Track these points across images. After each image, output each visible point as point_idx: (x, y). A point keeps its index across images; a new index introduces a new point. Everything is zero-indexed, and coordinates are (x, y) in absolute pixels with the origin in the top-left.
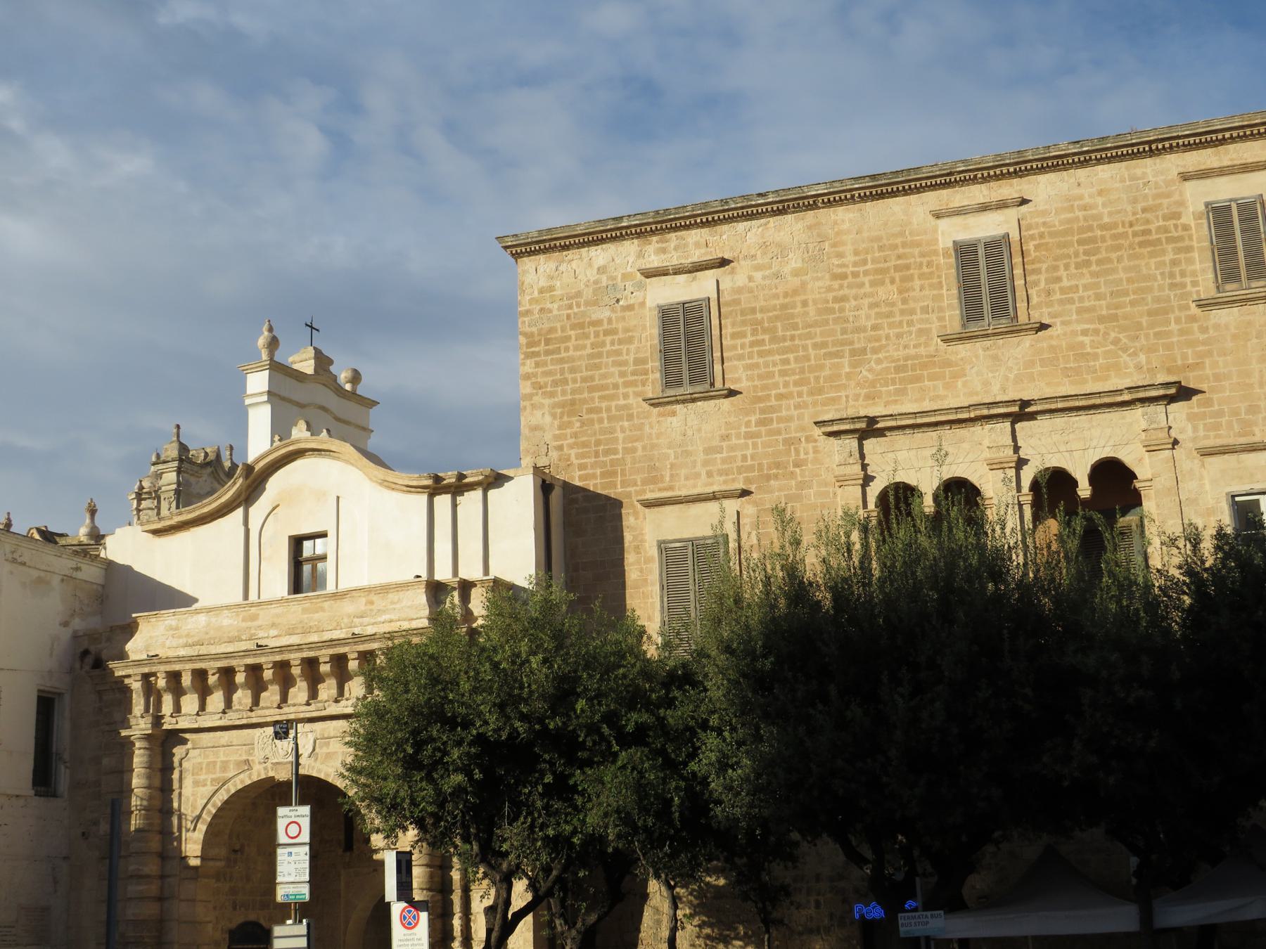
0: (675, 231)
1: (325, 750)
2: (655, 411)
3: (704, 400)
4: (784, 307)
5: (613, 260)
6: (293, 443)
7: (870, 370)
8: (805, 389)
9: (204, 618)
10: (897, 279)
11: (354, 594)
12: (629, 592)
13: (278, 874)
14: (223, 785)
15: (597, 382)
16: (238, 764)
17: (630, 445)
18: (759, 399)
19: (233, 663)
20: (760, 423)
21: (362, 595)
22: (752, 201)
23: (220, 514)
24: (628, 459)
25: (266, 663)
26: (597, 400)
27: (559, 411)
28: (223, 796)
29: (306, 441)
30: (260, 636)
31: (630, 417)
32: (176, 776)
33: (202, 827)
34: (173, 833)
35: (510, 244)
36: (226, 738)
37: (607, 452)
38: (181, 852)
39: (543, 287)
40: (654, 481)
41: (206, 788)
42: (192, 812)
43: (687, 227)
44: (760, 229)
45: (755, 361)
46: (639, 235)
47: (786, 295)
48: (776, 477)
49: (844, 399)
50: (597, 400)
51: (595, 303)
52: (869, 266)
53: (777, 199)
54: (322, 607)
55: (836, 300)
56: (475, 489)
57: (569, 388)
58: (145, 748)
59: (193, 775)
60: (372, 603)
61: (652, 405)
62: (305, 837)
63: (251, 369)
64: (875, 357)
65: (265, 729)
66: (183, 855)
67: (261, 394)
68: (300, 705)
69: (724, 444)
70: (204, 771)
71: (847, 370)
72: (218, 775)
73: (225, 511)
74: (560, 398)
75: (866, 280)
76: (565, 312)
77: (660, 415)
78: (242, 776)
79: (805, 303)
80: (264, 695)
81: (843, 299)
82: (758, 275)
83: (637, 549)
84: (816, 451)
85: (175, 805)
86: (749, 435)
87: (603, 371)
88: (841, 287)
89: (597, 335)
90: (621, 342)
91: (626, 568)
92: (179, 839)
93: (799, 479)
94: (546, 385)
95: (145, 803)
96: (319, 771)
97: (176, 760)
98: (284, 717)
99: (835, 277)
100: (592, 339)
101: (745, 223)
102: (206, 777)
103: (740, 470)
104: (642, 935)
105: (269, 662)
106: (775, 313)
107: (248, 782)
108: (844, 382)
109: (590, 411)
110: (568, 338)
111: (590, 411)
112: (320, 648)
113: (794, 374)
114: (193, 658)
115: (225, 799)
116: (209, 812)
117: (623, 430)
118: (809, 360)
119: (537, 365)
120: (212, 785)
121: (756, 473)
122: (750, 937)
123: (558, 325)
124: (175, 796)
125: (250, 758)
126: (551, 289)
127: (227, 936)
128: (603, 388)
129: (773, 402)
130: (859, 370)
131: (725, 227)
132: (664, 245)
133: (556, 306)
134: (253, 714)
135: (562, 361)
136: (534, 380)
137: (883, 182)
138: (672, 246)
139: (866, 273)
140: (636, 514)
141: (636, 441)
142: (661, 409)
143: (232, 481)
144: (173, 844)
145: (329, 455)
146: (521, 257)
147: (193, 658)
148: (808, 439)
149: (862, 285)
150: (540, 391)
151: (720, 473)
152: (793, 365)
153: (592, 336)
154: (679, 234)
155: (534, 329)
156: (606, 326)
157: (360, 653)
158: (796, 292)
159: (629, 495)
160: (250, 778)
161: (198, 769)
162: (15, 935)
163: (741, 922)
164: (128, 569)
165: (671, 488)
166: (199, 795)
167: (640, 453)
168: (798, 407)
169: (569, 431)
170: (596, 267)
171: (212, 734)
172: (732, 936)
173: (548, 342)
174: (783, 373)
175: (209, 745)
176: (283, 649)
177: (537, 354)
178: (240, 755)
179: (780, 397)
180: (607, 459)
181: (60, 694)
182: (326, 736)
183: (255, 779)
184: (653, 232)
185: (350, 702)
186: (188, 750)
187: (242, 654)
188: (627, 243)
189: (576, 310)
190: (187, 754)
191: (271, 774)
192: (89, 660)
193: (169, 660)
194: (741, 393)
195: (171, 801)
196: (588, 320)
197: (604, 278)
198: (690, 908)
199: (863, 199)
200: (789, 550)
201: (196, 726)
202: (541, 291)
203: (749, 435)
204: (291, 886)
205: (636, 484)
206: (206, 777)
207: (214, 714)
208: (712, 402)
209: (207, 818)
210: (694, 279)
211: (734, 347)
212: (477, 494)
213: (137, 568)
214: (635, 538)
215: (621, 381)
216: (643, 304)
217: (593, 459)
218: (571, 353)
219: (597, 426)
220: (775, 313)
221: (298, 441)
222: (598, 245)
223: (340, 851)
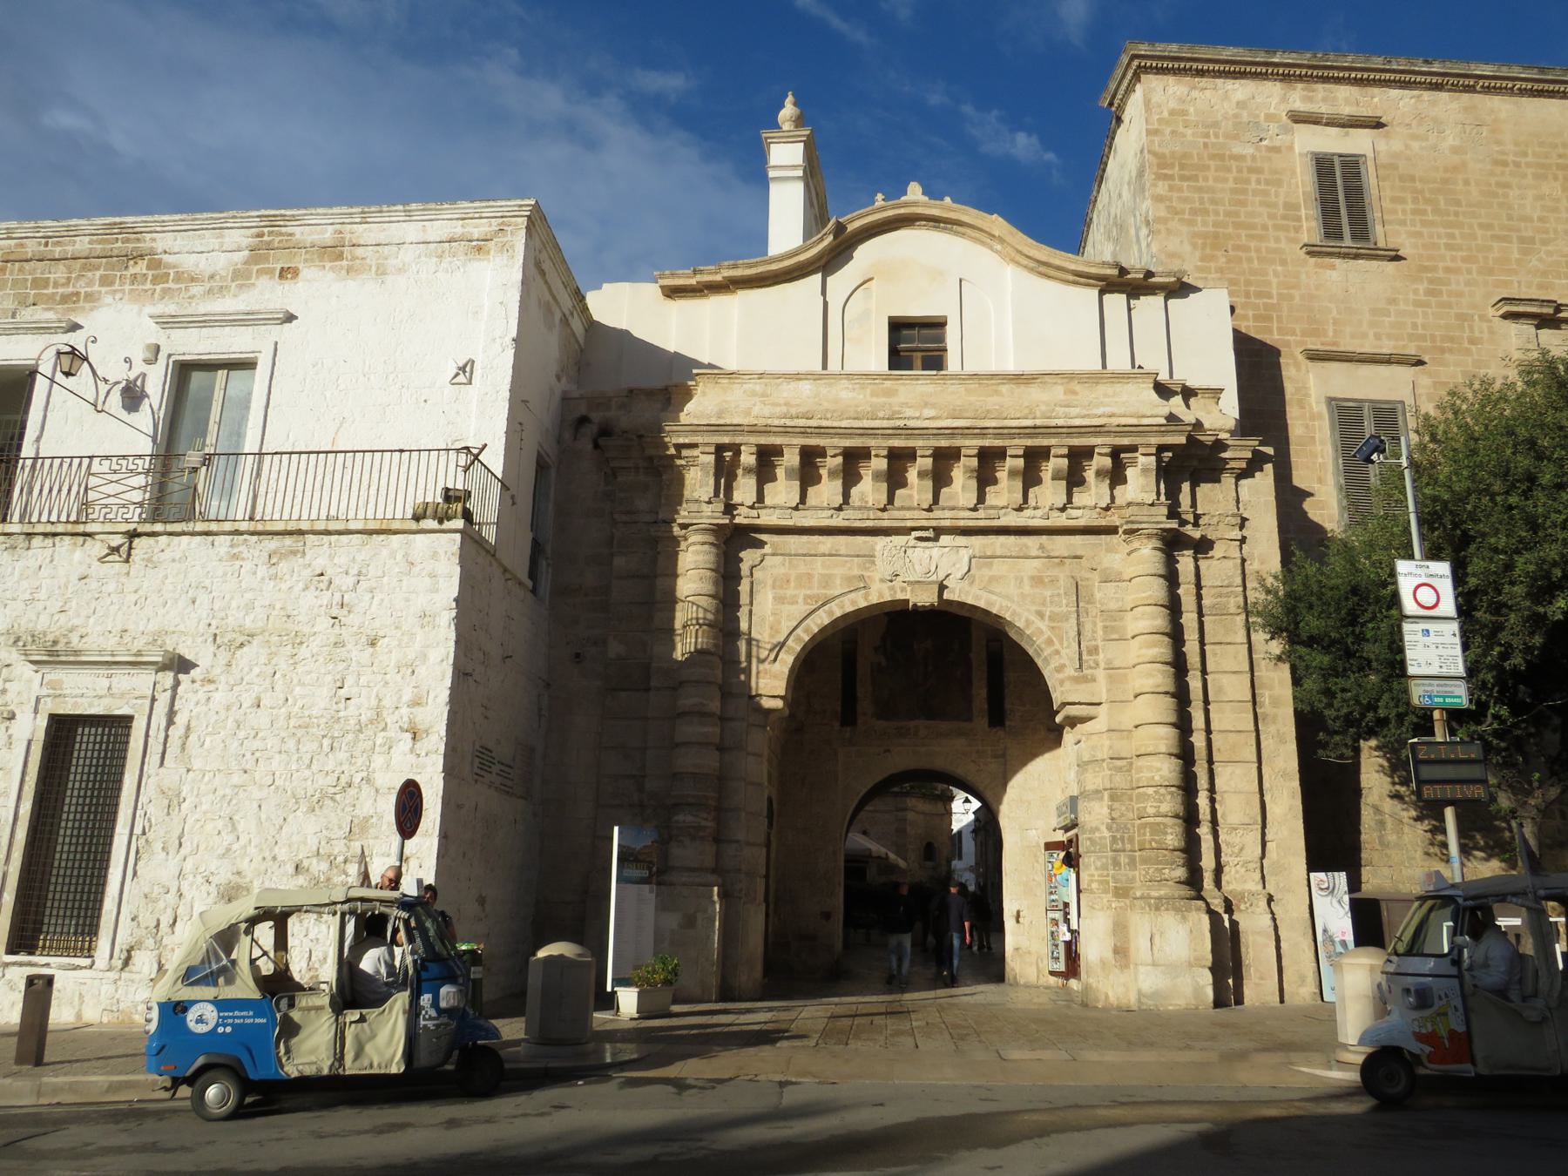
0: (1324, 82)
1: (986, 572)
2: (1313, 260)
3: (1367, 259)
4: (1445, 181)
5: (1254, 98)
6: (906, 205)
7: (1540, 260)
8: (1474, 267)
9: (808, 387)
10: (1560, 177)
11: (1047, 378)
12: (1292, 448)
13: (1409, 662)
14: (823, 605)
15: (1243, 218)
16: (849, 579)
17: (1285, 291)
18: (1426, 269)
19: (871, 442)
20: (1429, 293)
21: (1059, 381)
22: (1416, 66)
23: (789, 277)
24: (1285, 305)
25: (923, 448)
26: (1244, 238)
27: (1200, 242)
28: (822, 619)
29: (925, 205)
30: (907, 415)
31: (1283, 262)
32: (744, 588)
33: (787, 660)
34: (740, 663)
35: (1143, 53)
36: (829, 545)
37: (1259, 295)
38: (750, 688)
39: (1173, 110)
40: (1315, 333)
41: (794, 607)
42: (772, 636)
43: (1338, 80)
44: (1413, 100)
45: (1417, 229)
46: (1285, 78)
47: (1446, 170)
48: (1451, 351)
49: (1516, 285)
50: (1244, 238)
51: (1236, 137)
52: (1530, 159)
53: (1442, 71)
54: (996, 391)
55: (1498, 184)
56: (1155, 294)
57: (1211, 218)
58: (711, 544)
59: (774, 588)
60: (1075, 393)
61: (1308, 253)
62: (1448, 606)
63: (780, 137)
64: (1544, 248)
65: (894, 538)
66: (754, 693)
67: (794, 167)
68: (963, 509)
69: (1392, 308)
70: (792, 584)
71: (1517, 256)
72: (816, 591)
73: (796, 274)
74: (1200, 228)
75: (1530, 171)
76: (1202, 140)
77: (1316, 265)
78: (852, 595)
79: (1467, 182)
80: (899, 492)
81: (1507, 186)
82: (1415, 145)
83: (1301, 404)
84: (1491, 332)
85: (744, 626)
86: (1418, 304)
87: (1250, 209)
88: (1503, 173)
89: (1240, 171)
90: (1267, 182)
91: (1289, 422)
92: (748, 671)
93: (1476, 357)
94: (1183, 212)
95: (710, 616)
96: (977, 597)
97: (745, 568)
98: (934, 523)
99: (1496, 163)
100: (1235, 174)
101: (1397, 91)
102: (796, 592)
103: (1411, 337)
104: (1363, 837)
105: (928, 448)
106: (1436, 185)
107: (863, 604)
108: (1515, 267)
109: (1238, 248)
110: (1207, 168)
111: (1238, 248)
112: (1012, 436)
113: (1461, 249)
114: (809, 430)
116: (799, 639)
117: (1276, 274)
118: (1476, 239)
119: (1171, 188)
120: (806, 603)
121: (1429, 344)
122: (1492, 848)
123: (1195, 152)
124: (743, 614)
125: (866, 574)
126: (1184, 113)
128: (1252, 226)
129: (1441, 274)
130: (1529, 258)
131: (1376, 90)
132: (1311, 94)
133: (1189, 132)
134: (885, 515)
135: (1200, 189)
136: (1168, 203)
137: (1550, 77)
138: (1320, 96)
139: (1528, 165)
140: (1298, 366)
141: (1292, 288)
142: (1320, 260)
143: (820, 236)
144: (739, 678)
145: (951, 230)
146: (1148, 73)
147: (809, 430)
148: (1482, 318)
149: (1524, 176)
150: (1177, 217)
151: (1389, 336)
152: (1459, 241)
153: (1234, 170)
154: (1327, 86)
155: (1166, 151)
156: (1249, 162)
157: (1070, 448)
158: (1455, 169)
159: (1288, 344)
160: (866, 597)
161: (781, 582)
163: (1479, 830)
164: (624, 335)
165: (1334, 344)
167: (1297, 300)
168: (1468, 283)
169: (1213, 265)
170: (1234, 101)
171: (805, 538)
172: (1471, 845)
173: (1182, 167)
174: (1449, 247)
175: (801, 551)
176: (956, 431)
177: (1171, 177)
178: (850, 569)
179: (1448, 270)
180: (1260, 301)
182: (989, 554)
183: (874, 599)
184: (1300, 78)
185: (1039, 513)
186: (764, 555)
188: (1269, 84)
189: (1213, 140)
190: (762, 561)
191: (900, 596)
192: (590, 430)
193: (769, 429)
194: (1405, 259)
195: (737, 620)
196: (1228, 153)
197: (1245, 114)
198: (1415, 810)
199: (1523, 92)
200: (283, 664)
201: (790, 523)
202: (1172, 113)
203: (1418, 304)
204: (1435, 682)
205: (1294, 334)
206: (796, 592)
207: (823, 509)
208: (1375, 263)
209: (795, 646)
210: (1347, 134)
211: (1395, 212)
212: (1158, 300)
213: (637, 333)
214: (1298, 390)
215: (1270, 223)
216: (1291, 148)
217: (1243, 300)
218: (1211, 183)
219: (1245, 265)
220: (1436, 185)
221: (915, 204)
222: (1236, 78)
223: (837, 725)
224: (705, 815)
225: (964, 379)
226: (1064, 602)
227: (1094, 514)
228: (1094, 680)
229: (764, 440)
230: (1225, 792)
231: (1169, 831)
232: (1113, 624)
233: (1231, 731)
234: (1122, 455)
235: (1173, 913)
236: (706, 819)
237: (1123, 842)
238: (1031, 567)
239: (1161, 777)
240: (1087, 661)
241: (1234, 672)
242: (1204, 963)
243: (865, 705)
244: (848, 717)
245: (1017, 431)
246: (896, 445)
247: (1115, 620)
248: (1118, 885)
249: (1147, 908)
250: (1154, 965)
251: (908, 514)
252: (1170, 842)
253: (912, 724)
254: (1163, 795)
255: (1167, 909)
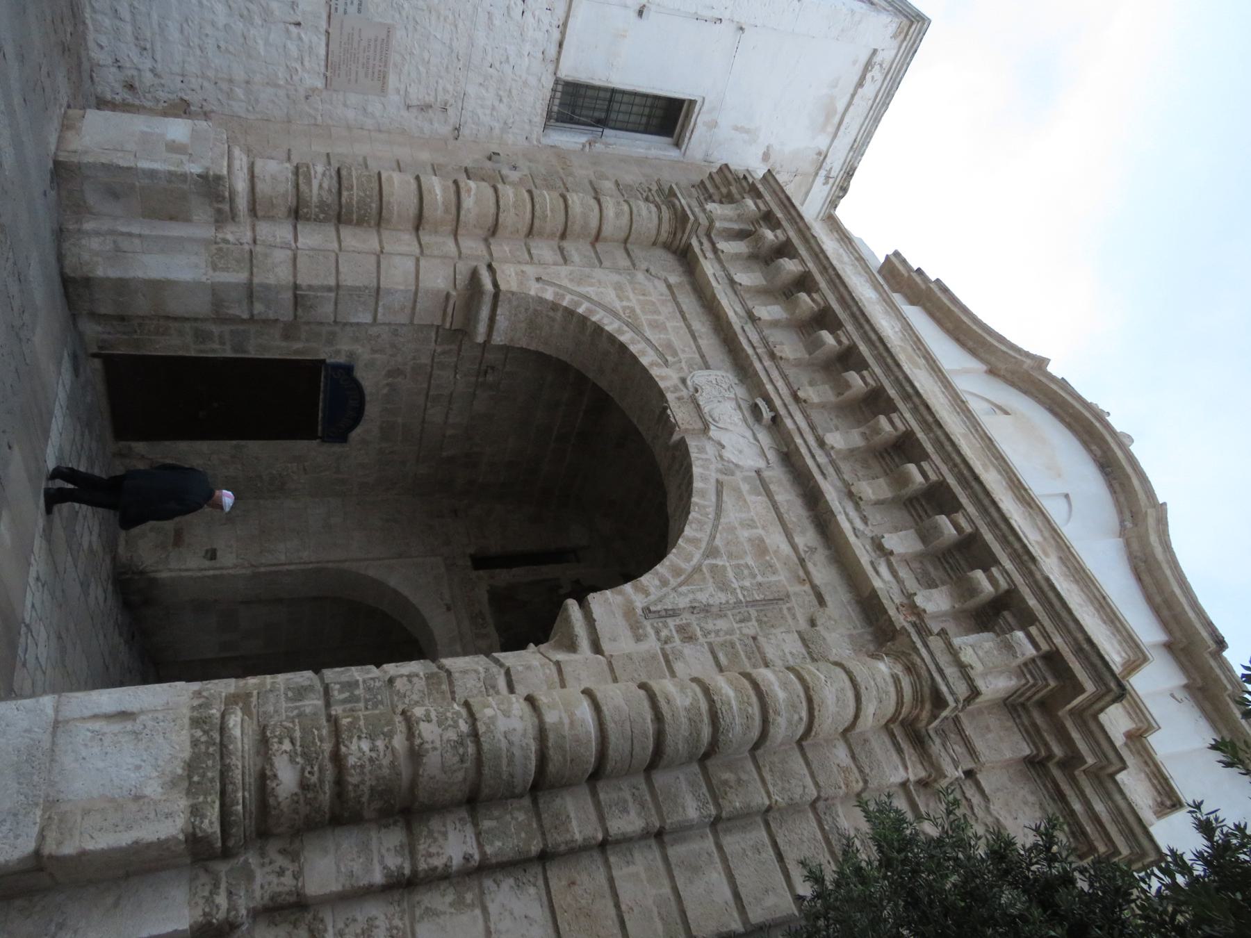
70: (641, 298)
98: (782, 411)
105: (876, 379)
112: (947, 459)
115: (607, 328)
127: (342, 360)
162: (345, 13)
166: (601, 289)
181: (677, 145)
183: (654, 372)
187: (874, 337)
223: (471, 550)
224: (325, 185)
225: (977, 430)
226: (747, 583)
227: (898, 599)
228: (638, 639)
229: (796, 241)
230: (485, 910)
231: (380, 744)
232: (742, 654)
233: (617, 906)
234: (1006, 613)
235: (186, 754)
236: (320, 186)
237: (344, 701)
238: (776, 540)
239: (493, 719)
240: (666, 625)
241: (737, 896)
242: (52, 836)
243: (504, 577)
244: (481, 562)
245: (958, 460)
246: (828, 497)
247: (749, 659)
248: (254, 700)
249: (196, 703)
250: (56, 724)
251: (780, 384)
252: (354, 747)
253: (491, 630)
254: (456, 725)
255: (195, 743)
